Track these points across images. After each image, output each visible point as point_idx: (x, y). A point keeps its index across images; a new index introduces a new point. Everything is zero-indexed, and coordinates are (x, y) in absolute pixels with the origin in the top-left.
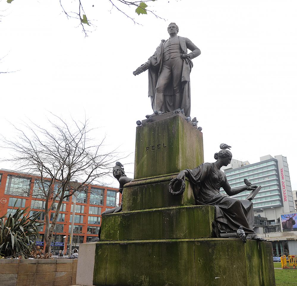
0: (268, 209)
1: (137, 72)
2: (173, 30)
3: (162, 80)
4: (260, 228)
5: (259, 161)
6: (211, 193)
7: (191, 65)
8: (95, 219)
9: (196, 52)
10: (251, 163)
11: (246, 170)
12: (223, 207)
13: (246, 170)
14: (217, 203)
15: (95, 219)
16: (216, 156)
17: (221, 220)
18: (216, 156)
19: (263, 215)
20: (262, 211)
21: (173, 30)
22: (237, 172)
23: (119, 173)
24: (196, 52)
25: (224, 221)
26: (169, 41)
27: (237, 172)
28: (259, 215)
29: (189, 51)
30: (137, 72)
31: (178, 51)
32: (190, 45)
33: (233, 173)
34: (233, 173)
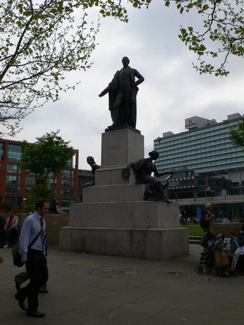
0: (230, 171)
1: (102, 95)
2: (126, 61)
3: (118, 102)
4: (223, 191)
5: (226, 119)
6: (146, 176)
7: (137, 89)
8: (15, 178)
9: (141, 79)
10: (218, 121)
11: (212, 129)
12: (151, 184)
13: (212, 129)
14: (148, 183)
15: (15, 178)
16: (150, 154)
17: (149, 192)
18: (150, 154)
19: (227, 177)
20: (226, 173)
21: (126, 61)
22: (203, 131)
23: (90, 161)
24: (141, 79)
25: (151, 192)
26: (123, 72)
27: (203, 131)
28: (224, 177)
29: (137, 79)
30: (102, 95)
31: (129, 80)
32: (136, 73)
33: (198, 132)
34: (198, 132)
